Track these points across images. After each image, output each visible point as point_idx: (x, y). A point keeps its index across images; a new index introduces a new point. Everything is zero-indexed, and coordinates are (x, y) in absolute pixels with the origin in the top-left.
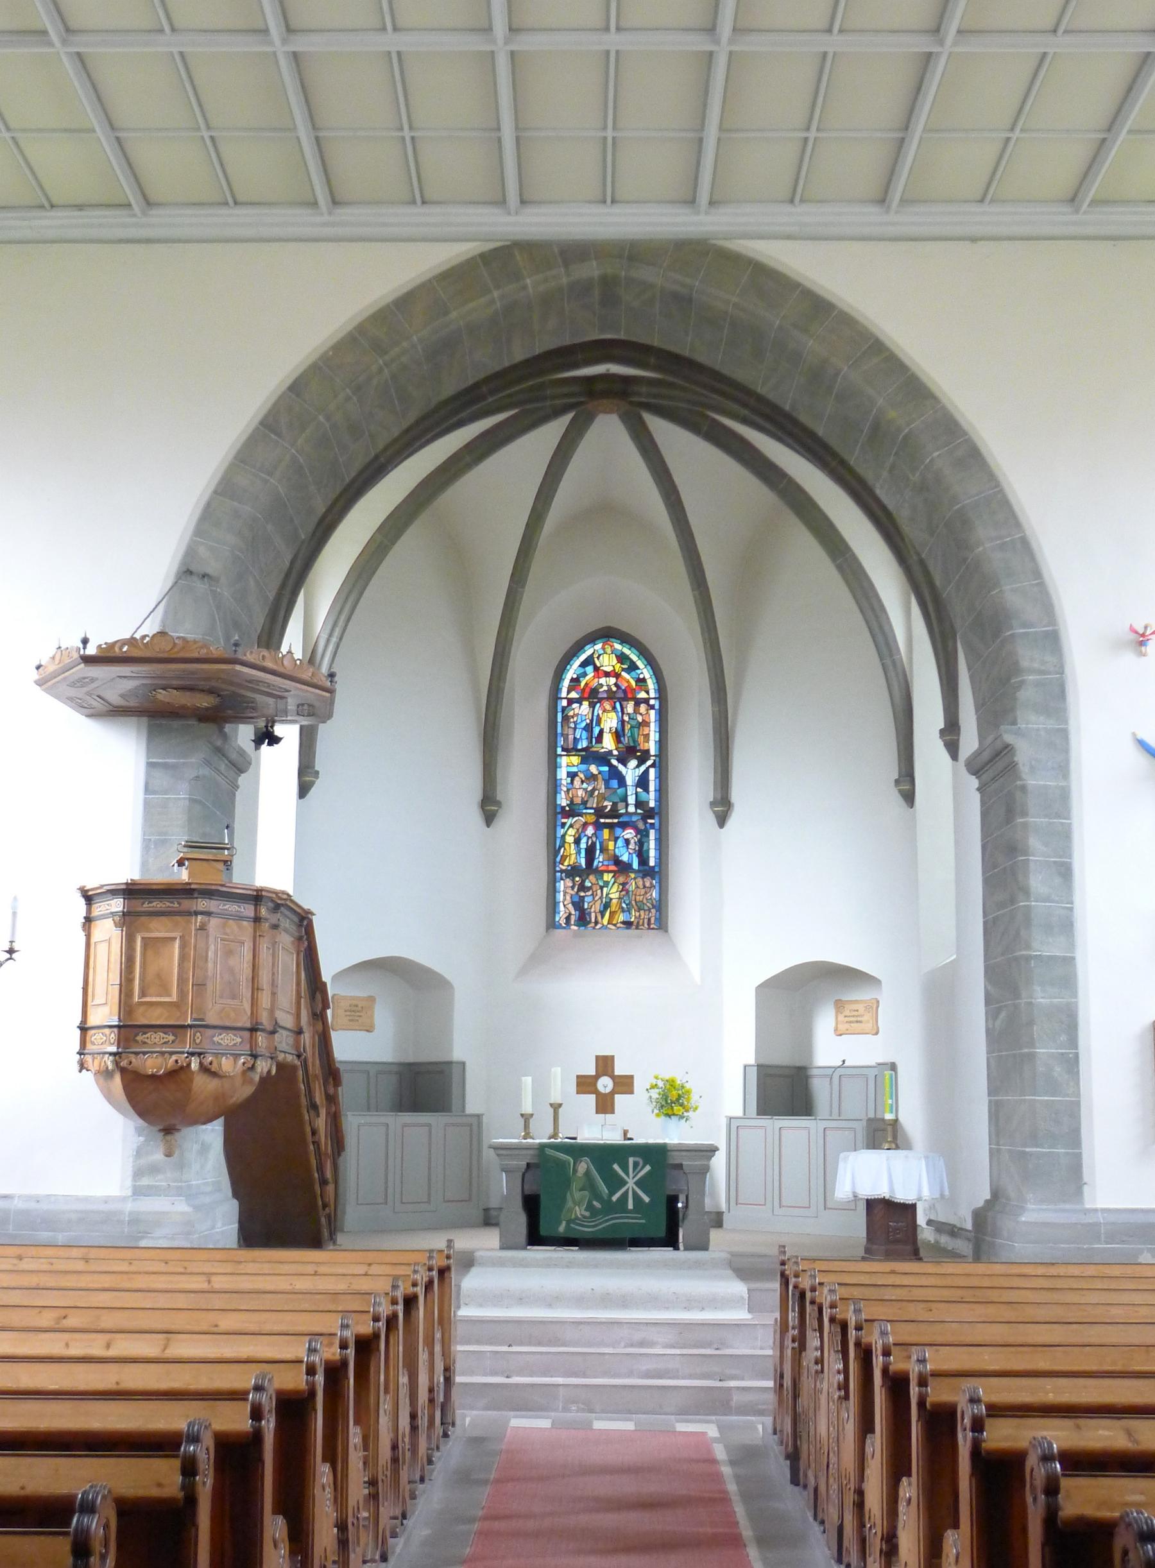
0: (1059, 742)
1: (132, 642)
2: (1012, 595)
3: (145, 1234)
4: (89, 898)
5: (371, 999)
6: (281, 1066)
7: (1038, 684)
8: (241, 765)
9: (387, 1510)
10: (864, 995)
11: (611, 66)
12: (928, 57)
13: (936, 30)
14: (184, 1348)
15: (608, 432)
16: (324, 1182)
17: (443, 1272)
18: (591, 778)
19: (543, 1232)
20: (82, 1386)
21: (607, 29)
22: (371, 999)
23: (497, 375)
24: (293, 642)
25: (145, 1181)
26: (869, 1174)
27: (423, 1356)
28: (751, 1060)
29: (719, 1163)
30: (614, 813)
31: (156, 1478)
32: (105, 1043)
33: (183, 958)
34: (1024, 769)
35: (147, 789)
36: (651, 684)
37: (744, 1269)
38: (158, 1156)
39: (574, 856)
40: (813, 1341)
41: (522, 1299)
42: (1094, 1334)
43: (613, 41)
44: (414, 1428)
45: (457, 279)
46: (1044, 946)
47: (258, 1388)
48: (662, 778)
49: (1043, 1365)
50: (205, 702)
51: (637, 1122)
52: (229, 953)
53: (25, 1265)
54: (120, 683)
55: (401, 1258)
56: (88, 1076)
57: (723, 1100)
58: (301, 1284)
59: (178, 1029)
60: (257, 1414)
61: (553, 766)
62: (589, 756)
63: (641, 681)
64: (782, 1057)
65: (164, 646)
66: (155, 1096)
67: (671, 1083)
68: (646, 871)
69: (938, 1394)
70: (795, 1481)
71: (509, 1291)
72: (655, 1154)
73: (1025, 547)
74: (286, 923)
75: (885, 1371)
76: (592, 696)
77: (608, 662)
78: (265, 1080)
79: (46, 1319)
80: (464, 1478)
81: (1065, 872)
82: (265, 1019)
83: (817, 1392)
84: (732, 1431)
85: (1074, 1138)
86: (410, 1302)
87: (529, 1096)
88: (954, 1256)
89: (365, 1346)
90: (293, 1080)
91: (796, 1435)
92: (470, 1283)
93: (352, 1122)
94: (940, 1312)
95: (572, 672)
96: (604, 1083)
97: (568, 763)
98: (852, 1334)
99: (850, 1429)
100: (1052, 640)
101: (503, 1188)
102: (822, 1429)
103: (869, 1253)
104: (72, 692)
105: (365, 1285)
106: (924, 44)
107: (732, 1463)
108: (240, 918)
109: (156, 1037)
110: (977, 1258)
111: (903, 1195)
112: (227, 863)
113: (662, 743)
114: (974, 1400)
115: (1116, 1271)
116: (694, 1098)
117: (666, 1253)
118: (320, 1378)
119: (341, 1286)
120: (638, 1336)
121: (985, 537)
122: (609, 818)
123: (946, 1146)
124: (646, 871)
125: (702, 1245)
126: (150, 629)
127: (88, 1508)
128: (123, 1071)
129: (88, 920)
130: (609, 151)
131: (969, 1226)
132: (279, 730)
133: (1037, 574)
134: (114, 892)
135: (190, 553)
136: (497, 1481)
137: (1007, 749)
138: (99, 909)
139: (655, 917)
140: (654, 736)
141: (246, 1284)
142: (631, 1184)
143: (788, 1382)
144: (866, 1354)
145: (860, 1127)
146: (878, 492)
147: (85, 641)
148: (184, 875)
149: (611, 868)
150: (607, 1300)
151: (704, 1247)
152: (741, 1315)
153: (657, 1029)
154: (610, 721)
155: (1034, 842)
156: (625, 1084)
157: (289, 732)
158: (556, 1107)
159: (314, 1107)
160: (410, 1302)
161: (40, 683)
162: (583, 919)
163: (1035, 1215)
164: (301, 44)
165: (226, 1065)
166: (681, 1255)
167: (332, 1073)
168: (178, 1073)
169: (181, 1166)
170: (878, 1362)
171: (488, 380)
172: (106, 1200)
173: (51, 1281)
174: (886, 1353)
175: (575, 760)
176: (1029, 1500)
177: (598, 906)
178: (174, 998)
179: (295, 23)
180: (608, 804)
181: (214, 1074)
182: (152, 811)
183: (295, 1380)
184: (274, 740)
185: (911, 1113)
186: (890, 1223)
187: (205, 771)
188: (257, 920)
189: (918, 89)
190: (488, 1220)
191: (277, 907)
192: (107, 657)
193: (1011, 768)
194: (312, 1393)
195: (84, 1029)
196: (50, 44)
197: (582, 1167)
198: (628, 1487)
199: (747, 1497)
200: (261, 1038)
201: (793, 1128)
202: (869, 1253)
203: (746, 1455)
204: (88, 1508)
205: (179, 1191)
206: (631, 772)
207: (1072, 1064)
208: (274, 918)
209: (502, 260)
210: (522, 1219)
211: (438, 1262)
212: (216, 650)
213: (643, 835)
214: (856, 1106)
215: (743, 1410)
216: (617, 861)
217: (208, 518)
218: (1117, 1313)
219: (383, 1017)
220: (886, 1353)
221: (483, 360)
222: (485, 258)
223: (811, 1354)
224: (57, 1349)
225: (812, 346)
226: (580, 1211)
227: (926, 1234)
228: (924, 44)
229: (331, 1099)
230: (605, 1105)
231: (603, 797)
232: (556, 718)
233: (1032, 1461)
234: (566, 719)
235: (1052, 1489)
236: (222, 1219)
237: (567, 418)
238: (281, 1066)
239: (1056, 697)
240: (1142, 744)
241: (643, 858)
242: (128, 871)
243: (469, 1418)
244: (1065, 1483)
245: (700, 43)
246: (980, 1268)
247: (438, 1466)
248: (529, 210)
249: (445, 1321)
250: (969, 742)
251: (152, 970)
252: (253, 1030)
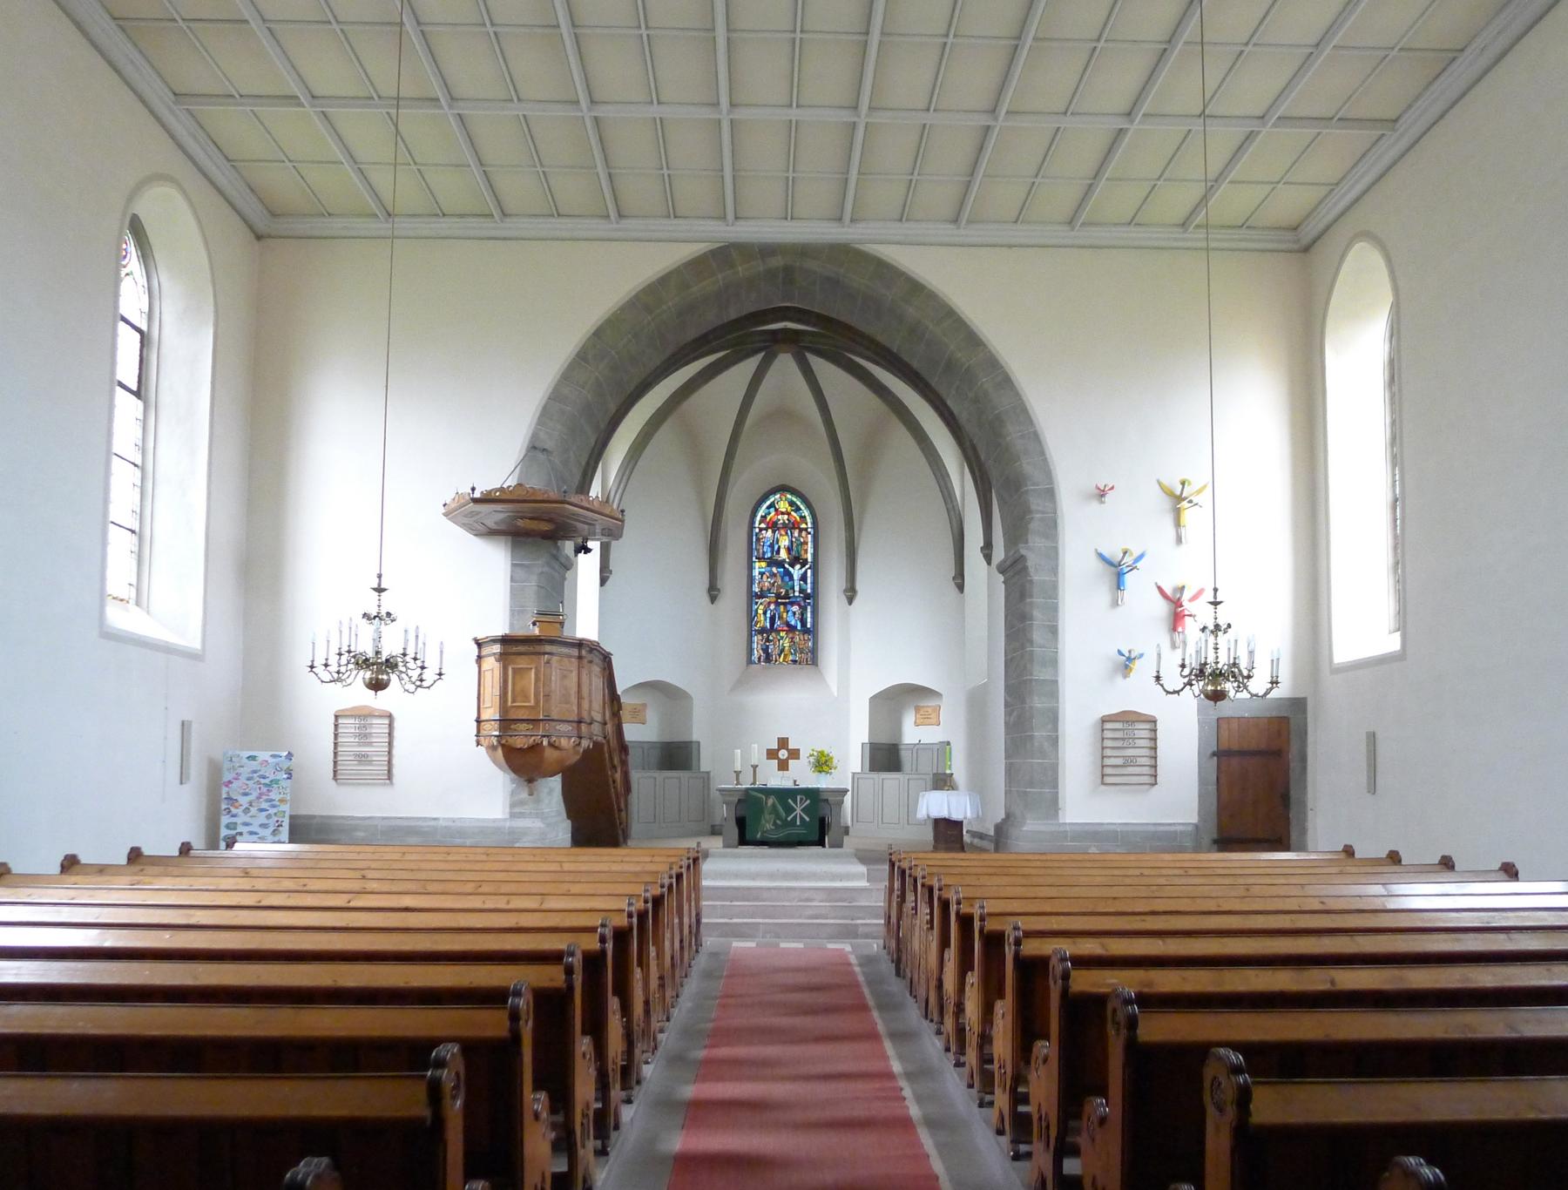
0: (1053, 555)
1: (501, 489)
2: (1028, 467)
3: (518, 840)
4: (479, 644)
5: (644, 705)
6: (596, 743)
7: (1042, 520)
8: (568, 566)
9: (669, 993)
10: (932, 703)
11: (793, 129)
12: (988, 128)
13: (993, 111)
14: (552, 903)
15: (785, 364)
16: (620, 810)
17: (696, 860)
18: (774, 575)
19: (748, 837)
20: (497, 925)
21: (791, 105)
22: (644, 705)
23: (723, 326)
24: (595, 490)
25: (517, 810)
26: (936, 804)
27: (686, 908)
28: (865, 738)
29: (848, 799)
30: (787, 596)
31: (551, 976)
32: (493, 730)
33: (537, 680)
34: (1031, 570)
35: (512, 580)
36: (809, 520)
37: (864, 857)
38: (524, 795)
39: (763, 622)
40: (910, 897)
41: (737, 876)
42: (1075, 892)
43: (794, 114)
44: (682, 948)
45: (697, 266)
46: (1040, 674)
47: (603, 926)
48: (815, 575)
49: (1048, 909)
50: (545, 527)
51: (802, 775)
52: (564, 677)
53: (450, 858)
54: (495, 515)
55: (672, 852)
56: (482, 749)
57: (851, 760)
58: (615, 867)
59: (535, 721)
60: (603, 940)
61: (751, 568)
62: (772, 562)
63: (803, 518)
64: (884, 739)
65: (521, 494)
66: (522, 761)
67: (822, 753)
68: (805, 631)
69: (991, 925)
70: (898, 974)
71: (731, 872)
72: (812, 794)
73: (1036, 437)
74: (597, 660)
75: (958, 913)
76: (773, 526)
77: (783, 506)
78: (587, 751)
79: (469, 888)
80: (708, 975)
81: (1054, 630)
82: (585, 715)
83: (913, 926)
84: (860, 947)
85: (1054, 784)
86: (679, 877)
87: (739, 759)
88: (982, 850)
89: (658, 901)
90: (602, 753)
91: (899, 950)
92: (706, 866)
93: (635, 776)
94: (984, 880)
95: (761, 512)
96: (783, 753)
97: (759, 567)
98: (936, 893)
99: (934, 946)
100: (1051, 494)
101: (723, 813)
102: (916, 945)
103: (936, 849)
104: (466, 520)
105: (653, 868)
106: (984, 120)
107: (860, 965)
108: (570, 656)
109: (523, 726)
110: (997, 850)
111: (956, 816)
112: (562, 624)
113: (815, 555)
114: (1016, 928)
115: (1080, 857)
116: (835, 761)
117: (818, 849)
118: (635, 920)
119: (638, 868)
120: (806, 895)
121: (1012, 431)
122: (783, 599)
123: (978, 787)
124: (805, 631)
125: (840, 846)
126: (512, 482)
127: (517, 993)
128: (503, 746)
129: (480, 657)
130: (790, 186)
131: (992, 833)
132: (590, 544)
133: (1042, 453)
134: (494, 641)
135: (535, 436)
136: (728, 977)
137: (1022, 558)
138: (485, 651)
139: (810, 658)
140: (810, 551)
141: (584, 867)
142: (798, 811)
143: (894, 919)
144: (945, 905)
145: (929, 778)
146: (949, 402)
147: (473, 489)
148: (536, 631)
149: (785, 630)
150: (786, 876)
151: (840, 846)
152: (864, 884)
153: (816, 720)
154: (784, 542)
155: (1036, 613)
156: (795, 754)
157: (594, 545)
158: (755, 767)
159: (614, 767)
160: (679, 877)
161: (446, 515)
162: (768, 659)
163: (1031, 827)
164: (600, 111)
165: (564, 742)
166: (827, 850)
167: (623, 748)
168: (535, 748)
169: (538, 801)
170: (953, 908)
171: (715, 330)
172: (494, 821)
173: (468, 866)
174: (959, 903)
175: (764, 564)
176: (1051, 983)
177: (777, 651)
178: (532, 703)
179: (597, 97)
180: (783, 591)
181: (556, 748)
182: (515, 593)
183: (622, 921)
184: (588, 551)
185: (958, 767)
186: (948, 832)
187: (546, 569)
188: (580, 657)
189: (981, 148)
190: (715, 831)
191: (591, 650)
192: (486, 499)
193: (1025, 568)
194: (631, 929)
195: (479, 721)
196: (441, 107)
197: (770, 802)
198: (801, 979)
199: (870, 983)
200: (583, 727)
201: (890, 778)
202: (936, 849)
203: (867, 961)
204: (517, 993)
205: (537, 816)
206: (796, 572)
207: (1055, 741)
208: (590, 657)
209: (724, 255)
210: (735, 832)
211: (693, 854)
212: (553, 495)
213: (804, 609)
214: (927, 767)
215: (866, 936)
216: (788, 624)
217: (545, 414)
218: (1083, 880)
219: (652, 716)
220: (959, 903)
221: (711, 318)
222: (713, 253)
223: (909, 903)
224: (479, 905)
225: (911, 312)
226: (769, 826)
227: (967, 838)
228: (984, 120)
229: (624, 763)
230: (783, 766)
231: (779, 587)
232: (752, 539)
233: (1054, 961)
234: (758, 540)
235: (1066, 976)
236: (562, 831)
237: (760, 356)
238: (596, 743)
239: (1051, 527)
240: (1101, 556)
241: (803, 623)
242: (501, 629)
243: (709, 941)
244: (1073, 973)
245: (846, 116)
246: (997, 856)
247: (694, 969)
248: (742, 222)
249: (696, 887)
250: (999, 554)
251: (518, 688)
252: (580, 722)
